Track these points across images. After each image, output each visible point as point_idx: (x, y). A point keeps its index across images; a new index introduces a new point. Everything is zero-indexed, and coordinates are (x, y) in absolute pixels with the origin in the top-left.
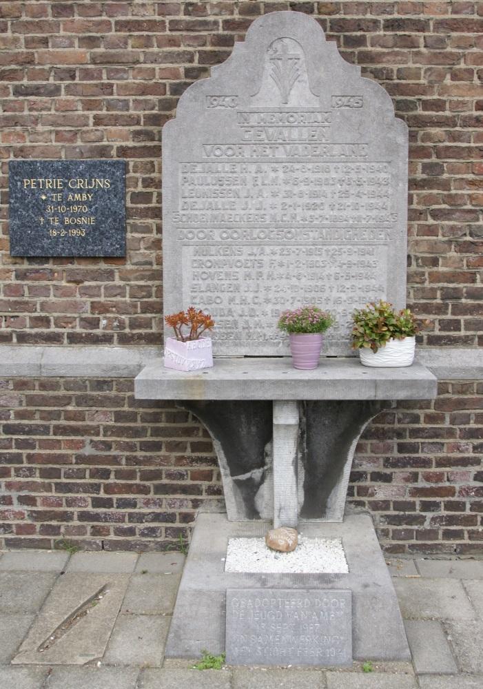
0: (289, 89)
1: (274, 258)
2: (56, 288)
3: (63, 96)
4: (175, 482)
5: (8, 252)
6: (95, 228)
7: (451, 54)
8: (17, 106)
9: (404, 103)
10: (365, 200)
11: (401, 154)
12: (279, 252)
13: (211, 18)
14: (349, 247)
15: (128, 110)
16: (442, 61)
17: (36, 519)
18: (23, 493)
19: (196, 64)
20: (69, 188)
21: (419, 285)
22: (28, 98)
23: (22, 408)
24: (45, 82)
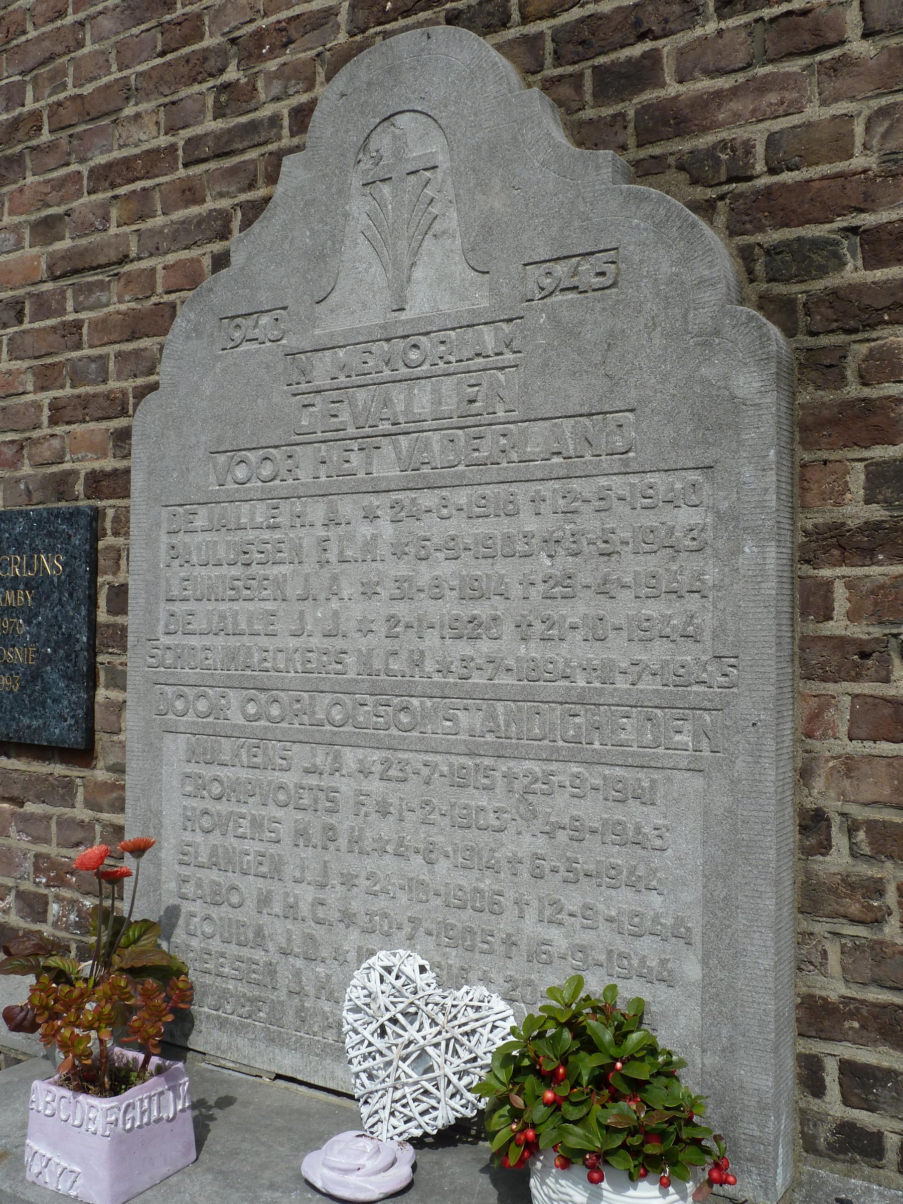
0: (407, 262)
1: (366, 786)
9: (792, 252)
10: (624, 607)
11: (750, 436)
12: (377, 768)
14: (575, 769)
15: (105, 381)
21: (861, 931)
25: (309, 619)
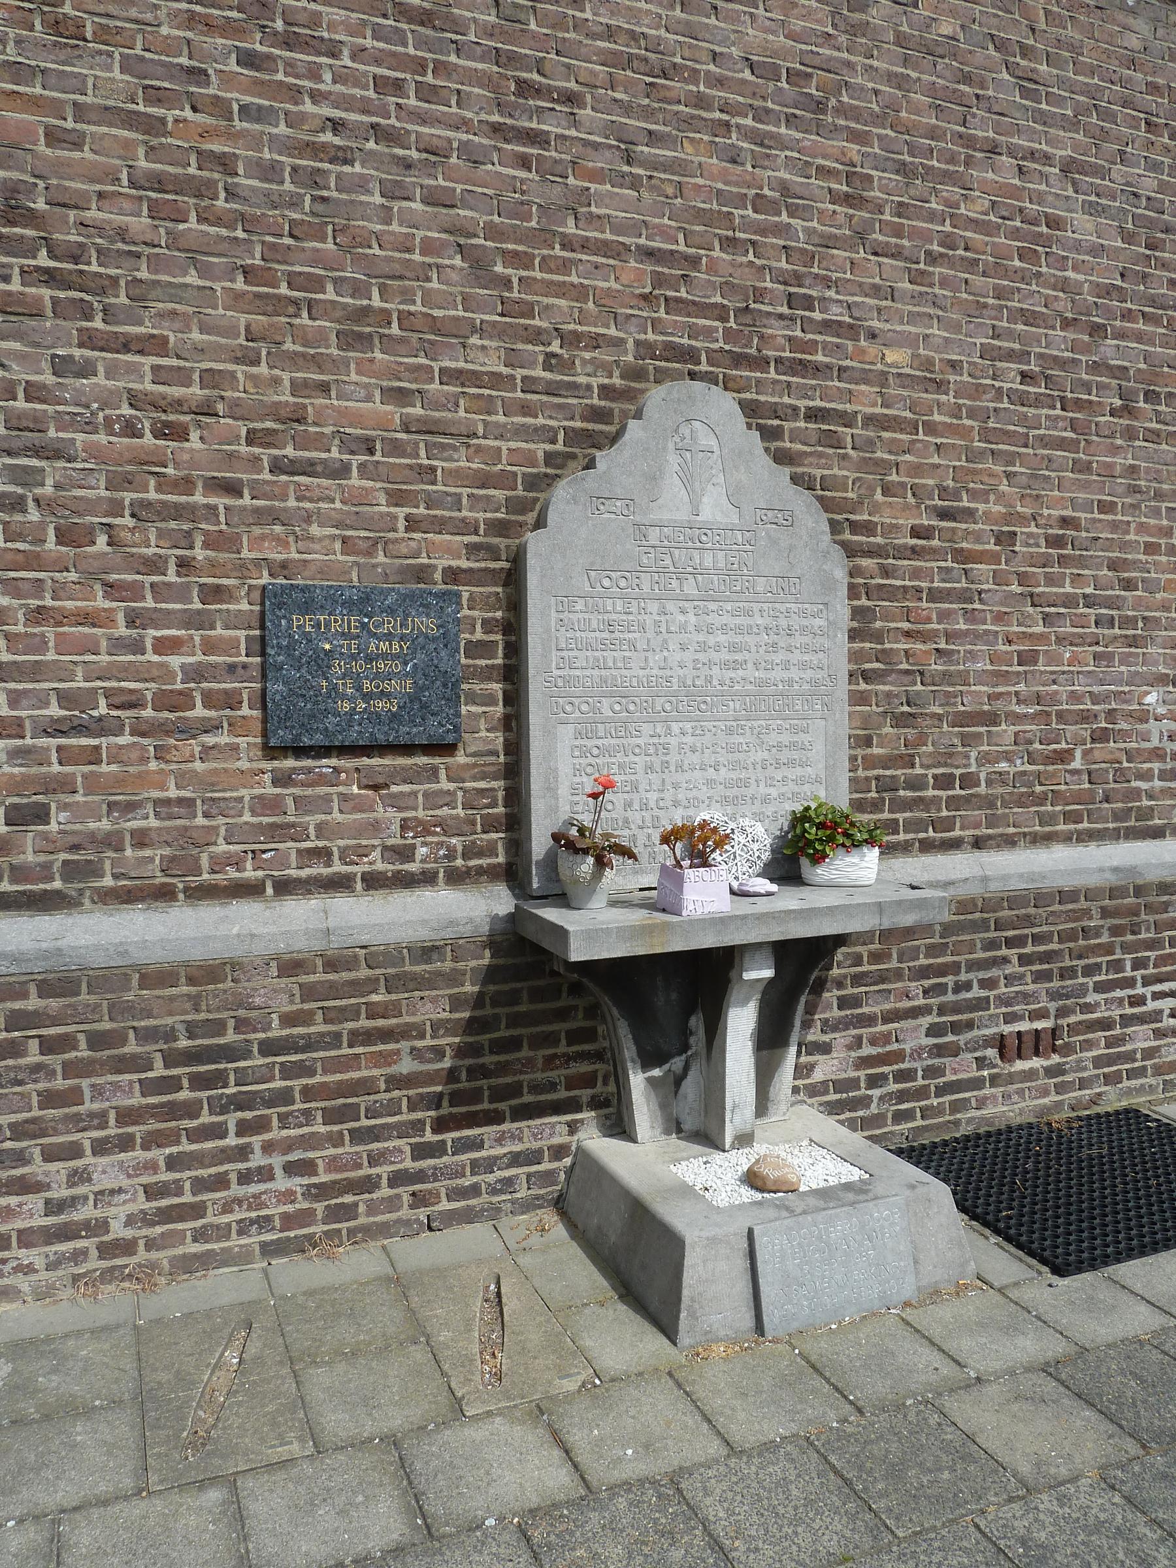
1: (684, 740)
2: (344, 798)
3: (355, 481)
4: (542, 1098)
5: (259, 740)
6: (413, 698)
7: (883, 460)
8: (277, 490)
13: (582, 380)
16: (872, 469)
17: (317, 1198)
18: (294, 1156)
19: (559, 447)
20: (369, 631)
22: (296, 478)
23: (294, 1007)
24: (324, 455)
25: (650, 660)
